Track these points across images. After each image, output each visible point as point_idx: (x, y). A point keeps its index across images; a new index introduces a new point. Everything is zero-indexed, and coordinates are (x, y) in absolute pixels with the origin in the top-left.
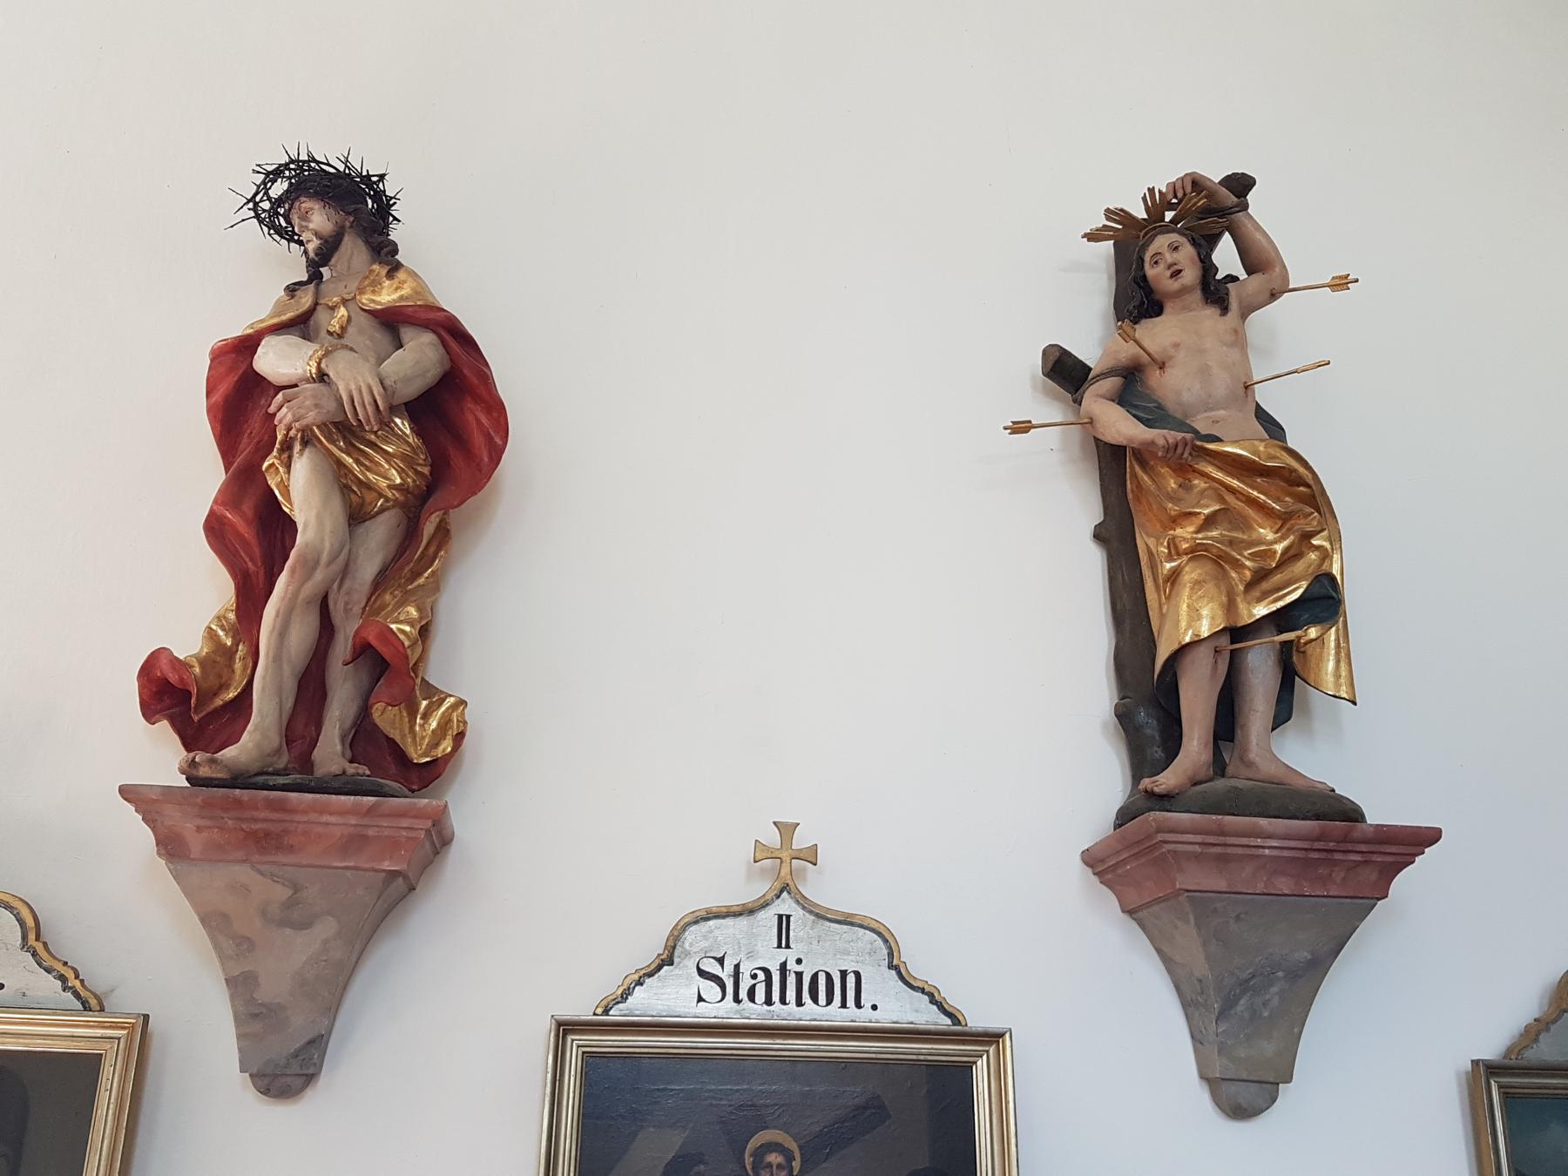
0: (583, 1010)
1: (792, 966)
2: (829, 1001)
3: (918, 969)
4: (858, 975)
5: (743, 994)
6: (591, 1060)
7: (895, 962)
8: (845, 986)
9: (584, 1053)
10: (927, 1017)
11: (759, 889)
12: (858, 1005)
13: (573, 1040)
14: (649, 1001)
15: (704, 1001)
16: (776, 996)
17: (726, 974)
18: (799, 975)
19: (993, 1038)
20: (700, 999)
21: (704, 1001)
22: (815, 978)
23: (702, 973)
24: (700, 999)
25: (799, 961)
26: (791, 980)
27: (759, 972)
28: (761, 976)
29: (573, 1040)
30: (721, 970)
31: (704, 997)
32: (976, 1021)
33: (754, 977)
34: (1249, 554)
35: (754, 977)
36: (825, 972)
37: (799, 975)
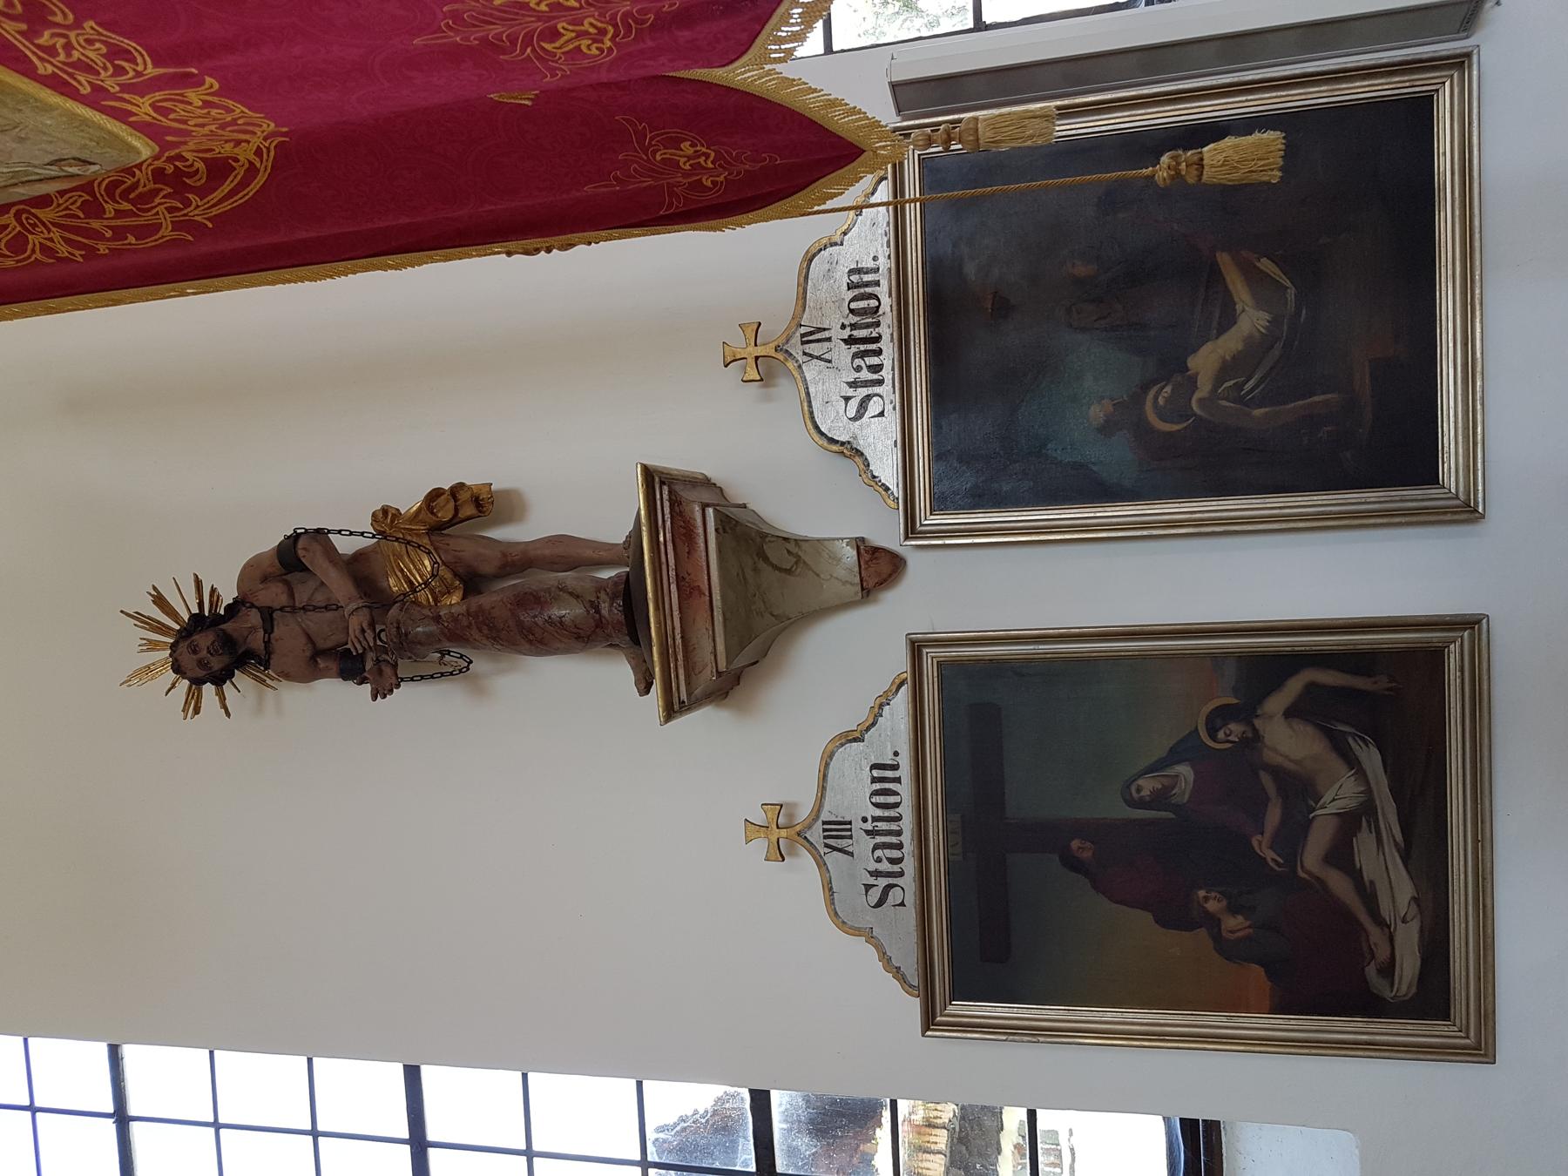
0: (914, 1005)
1: (869, 826)
2: (895, 793)
3: (862, 715)
4: (874, 767)
5: (896, 868)
6: (940, 503)
7: (857, 735)
8: (883, 772)
9: (931, 514)
10: (902, 699)
11: (807, 860)
12: (895, 767)
13: (927, 653)
14: (887, 469)
15: (903, 901)
16: (894, 840)
17: (883, 882)
18: (854, 326)
19: (916, 648)
20: (902, 904)
21: (903, 901)
22: (877, 805)
23: (880, 903)
24: (902, 904)
25: (865, 820)
26: (882, 826)
27: (876, 855)
28: (879, 853)
29: (921, 525)
30: (875, 888)
31: (900, 901)
32: (900, 662)
33: (879, 860)
34: (125, 182)
35: (858, 369)
36: (873, 852)
37: (875, 819)
